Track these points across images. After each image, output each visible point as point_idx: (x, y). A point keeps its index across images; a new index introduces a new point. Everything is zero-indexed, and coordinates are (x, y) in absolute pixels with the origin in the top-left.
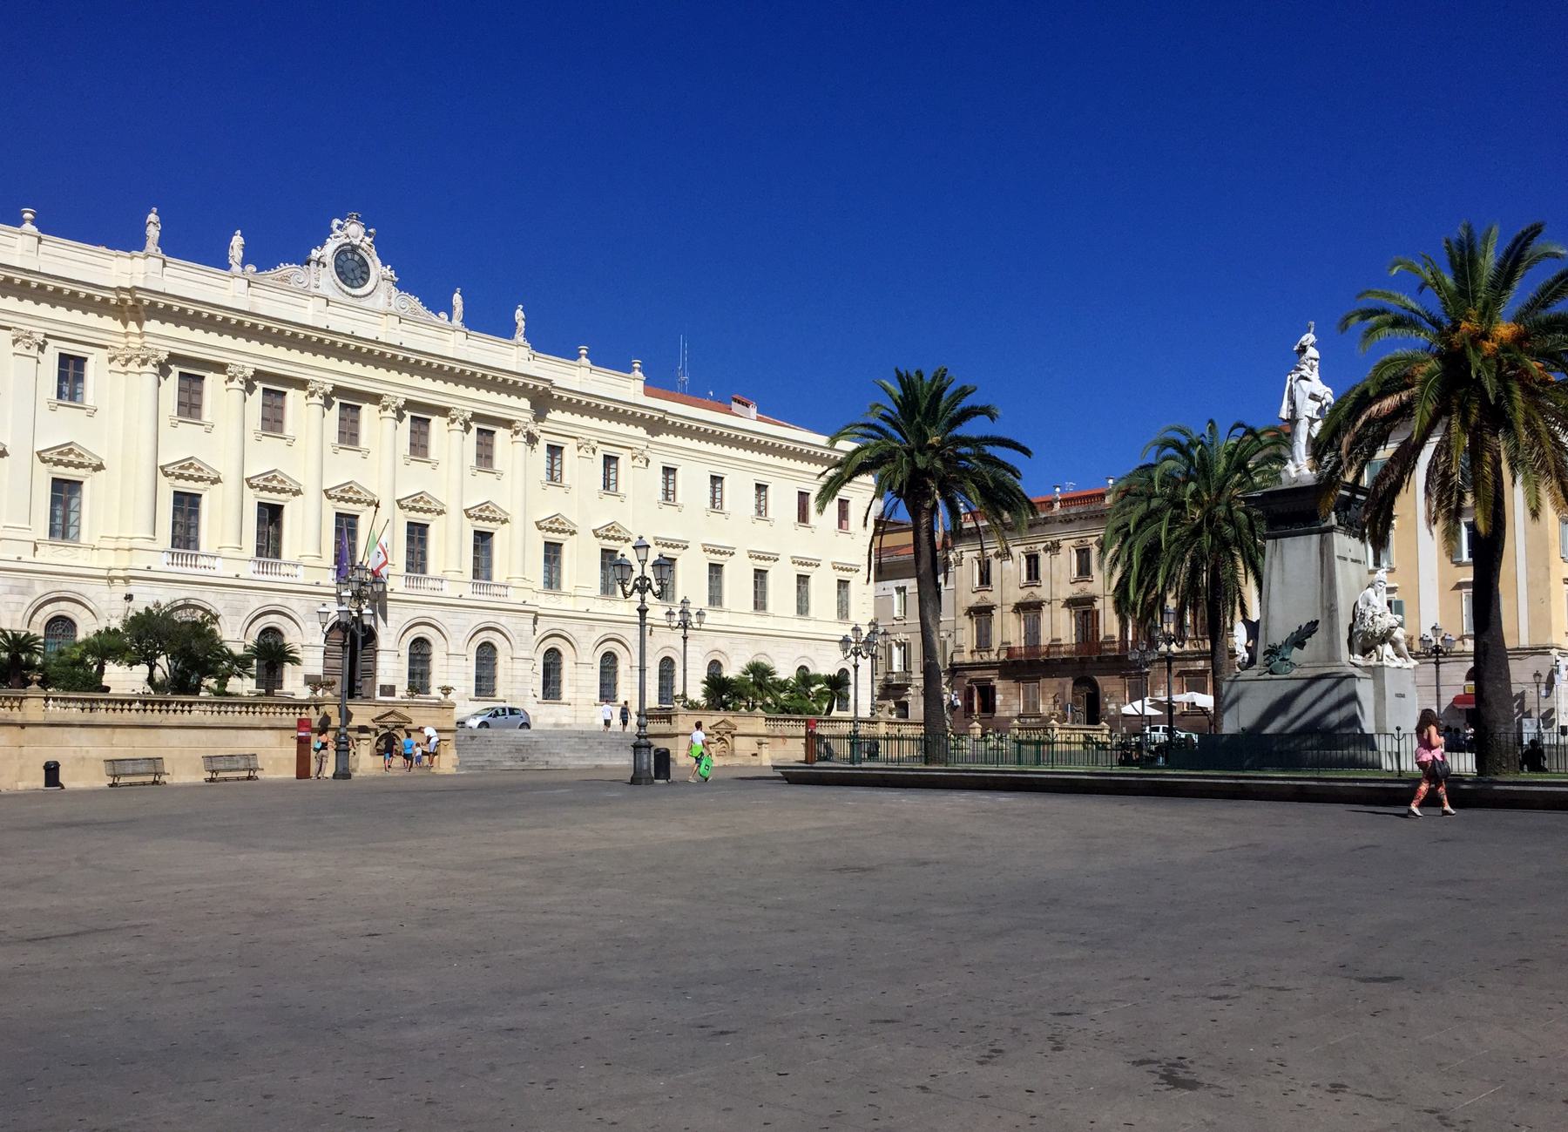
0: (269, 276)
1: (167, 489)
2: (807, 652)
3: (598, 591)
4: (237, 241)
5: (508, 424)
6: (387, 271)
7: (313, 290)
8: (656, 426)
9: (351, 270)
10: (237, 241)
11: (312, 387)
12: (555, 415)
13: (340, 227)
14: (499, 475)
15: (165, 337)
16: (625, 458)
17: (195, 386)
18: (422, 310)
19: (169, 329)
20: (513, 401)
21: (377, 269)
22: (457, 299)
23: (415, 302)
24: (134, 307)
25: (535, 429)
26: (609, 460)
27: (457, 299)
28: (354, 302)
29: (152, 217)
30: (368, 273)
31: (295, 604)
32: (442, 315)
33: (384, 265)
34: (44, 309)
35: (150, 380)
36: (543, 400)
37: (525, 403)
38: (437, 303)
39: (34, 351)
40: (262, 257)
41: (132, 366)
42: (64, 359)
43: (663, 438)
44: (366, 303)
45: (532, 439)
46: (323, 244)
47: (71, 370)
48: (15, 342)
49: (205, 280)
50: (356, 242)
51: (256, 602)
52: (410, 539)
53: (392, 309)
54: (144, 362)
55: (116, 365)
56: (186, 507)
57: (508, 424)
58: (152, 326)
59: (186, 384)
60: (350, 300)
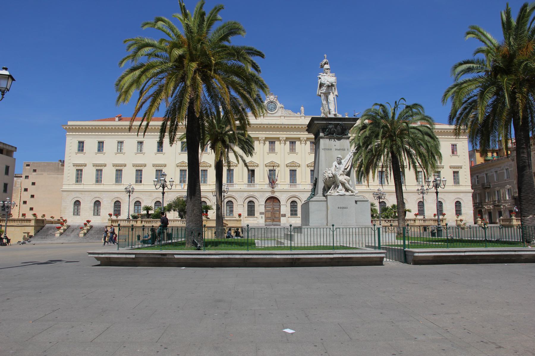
1: (267, 169)
2: (80, 196)
3: (94, 182)
6: (281, 105)
11: (260, 138)
14: (276, 154)
18: (292, 113)
21: (279, 105)
22: (302, 108)
23: (290, 111)
27: (302, 108)
31: (256, 194)
38: (296, 110)
51: (246, 194)
52: (291, 175)
56: (99, 173)
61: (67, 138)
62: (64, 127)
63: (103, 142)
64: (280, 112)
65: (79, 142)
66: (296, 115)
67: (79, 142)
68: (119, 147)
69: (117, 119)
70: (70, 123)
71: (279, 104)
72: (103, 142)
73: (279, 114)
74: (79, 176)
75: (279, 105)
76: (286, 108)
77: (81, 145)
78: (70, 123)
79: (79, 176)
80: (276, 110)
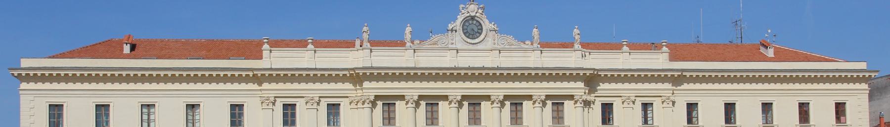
0: (426, 45)
4: (408, 29)
5: (571, 97)
6: (492, 26)
7: (450, 46)
8: (678, 79)
9: (472, 29)
10: (408, 29)
11: (450, 98)
12: (603, 86)
13: (463, 8)
15: (372, 88)
16: (657, 103)
17: (477, 108)
19: (374, 84)
20: (572, 84)
23: (510, 39)
24: (357, 77)
25: (590, 98)
26: (646, 106)
28: (475, 47)
29: (576, 31)
30: (482, 29)
32: (528, 42)
33: (490, 22)
34: (318, 86)
35: (367, 111)
36: (592, 80)
37: (581, 84)
38: (523, 36)
39: (271, 106)
40: (422, 36)
41: (360, 105)
42: (285, 106)
43: (685, 86)
44: (479, 47)
45: (587, 104)
46: (455, 19)
47: (333, 109)
48: (663, 102)
49: (392, 54)
50: (473, 14)
53: (496, 46)
54: (363, 103)
55: (353, 105)
57: (571, 97)
58: (366, 84)
59: (555, 108)
60: (471, 47)
61: (22, 98)
62: (16, 73)
63: (59, 107)
64: (490, 38)
65: (97, 106)
66: (523, 46)
67: (97, 106)
68: (145, 117)
69: (127, 49)
70: (25, 63)
71: (487, 21)
72: (59, 107)
73: (489, 43)
74: (237, 119)
75: (487, 25)
76: (501, 30)
77: (289, 112)
78: (25, 63)
79: (237, 119)
80: (482, 36)
